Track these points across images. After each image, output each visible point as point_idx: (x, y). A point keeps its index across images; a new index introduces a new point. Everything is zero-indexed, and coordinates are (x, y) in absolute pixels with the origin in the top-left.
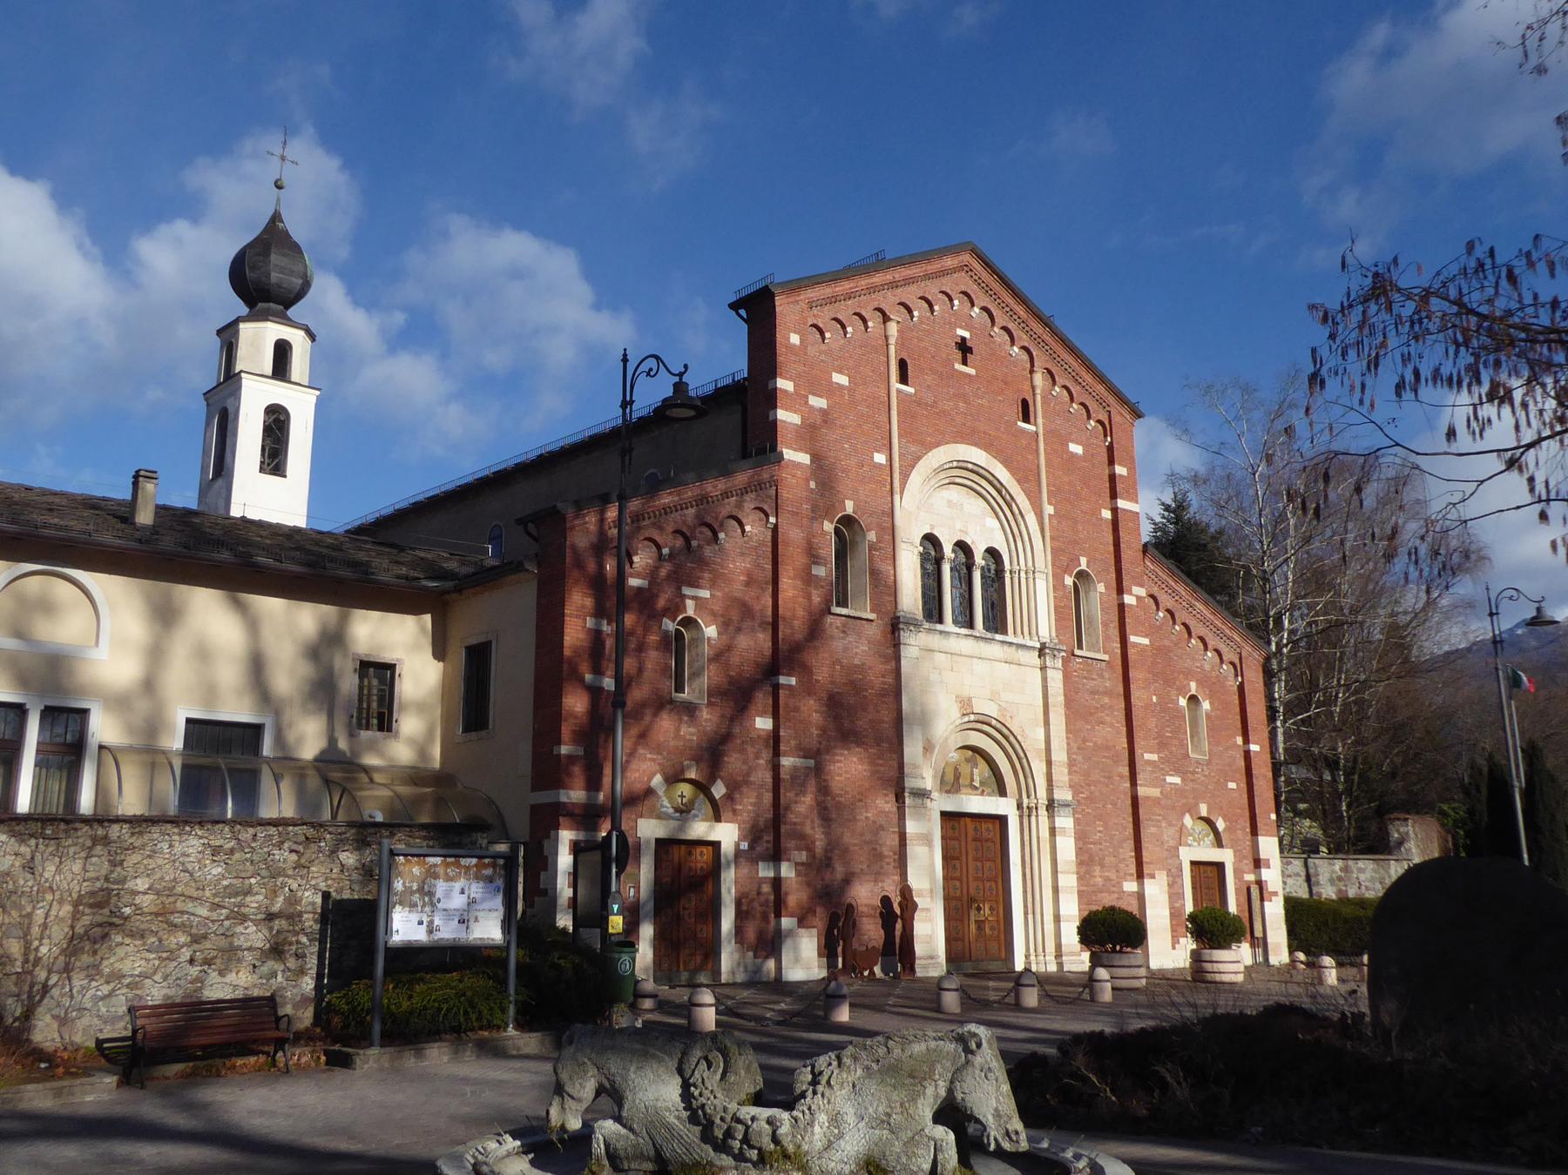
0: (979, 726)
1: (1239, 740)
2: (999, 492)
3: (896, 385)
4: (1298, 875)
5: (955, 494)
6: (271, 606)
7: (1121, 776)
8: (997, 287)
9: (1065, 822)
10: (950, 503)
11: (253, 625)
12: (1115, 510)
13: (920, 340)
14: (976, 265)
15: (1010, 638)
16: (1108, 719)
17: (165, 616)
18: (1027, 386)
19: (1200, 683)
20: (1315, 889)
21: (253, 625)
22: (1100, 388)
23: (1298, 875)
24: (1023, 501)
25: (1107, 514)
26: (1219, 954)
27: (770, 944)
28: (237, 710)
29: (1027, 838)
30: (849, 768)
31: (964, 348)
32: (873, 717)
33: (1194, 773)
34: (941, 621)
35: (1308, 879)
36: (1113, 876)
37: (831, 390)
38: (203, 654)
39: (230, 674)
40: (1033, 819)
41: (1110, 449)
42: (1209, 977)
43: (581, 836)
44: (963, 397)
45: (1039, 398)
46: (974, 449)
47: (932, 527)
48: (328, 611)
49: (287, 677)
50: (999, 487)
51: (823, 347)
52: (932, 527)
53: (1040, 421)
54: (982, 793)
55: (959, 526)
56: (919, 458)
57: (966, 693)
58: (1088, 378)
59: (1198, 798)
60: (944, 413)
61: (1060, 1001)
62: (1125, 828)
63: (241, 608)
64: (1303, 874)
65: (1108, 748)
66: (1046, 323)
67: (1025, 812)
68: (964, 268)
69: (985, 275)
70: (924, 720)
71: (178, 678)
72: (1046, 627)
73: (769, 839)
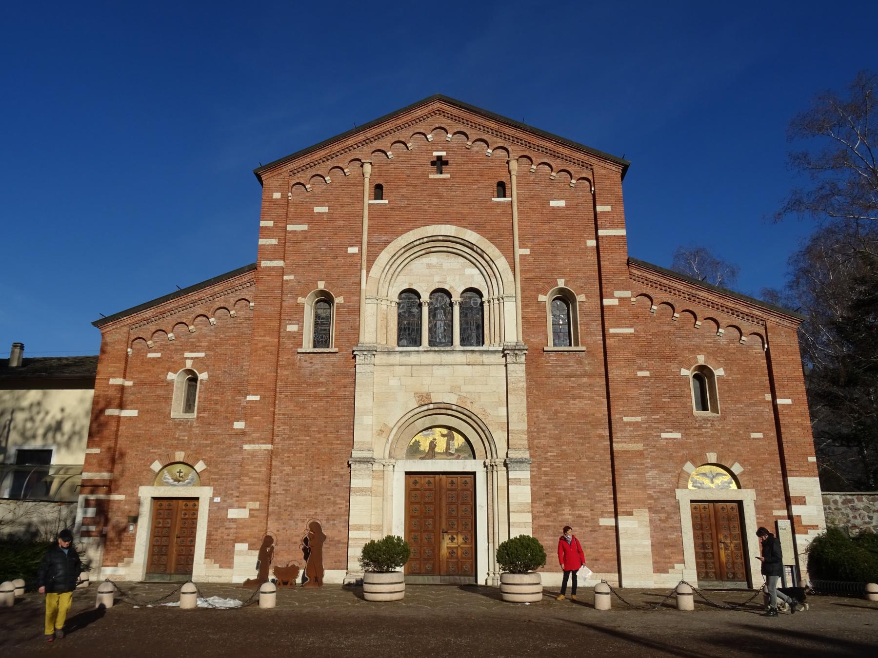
0: (438, 411)
1: (768, 397)
2: (473, 250)
3: (368, 201)
5: (433, 259)
7: (601, 436)
9: (523, 474)
10: (429, 266)
12: (597, 238)
15: (485, 348)
18: (504, 172)
19: (708, 355)
24: (492, 250)
25: (592, 243)
26: (517, 578)
29: (490, 487)
31: (440, 164)
34: (417, 342)
36: (587, 513)
40: (495, 473)
42: (369, 596)
45: (514, 178)
46: (443, 226)
47: (412, 284)
50: (471, 246)
51: (308, 194)
52: (451, 287)
54: (458, 458)
57: (425, 390)
60: (417, 209)
61: (710, 605)
62: (604, 477)
65: (585, 416)
67: (490, 468)
68: (440, 112)
72: (512, 333)
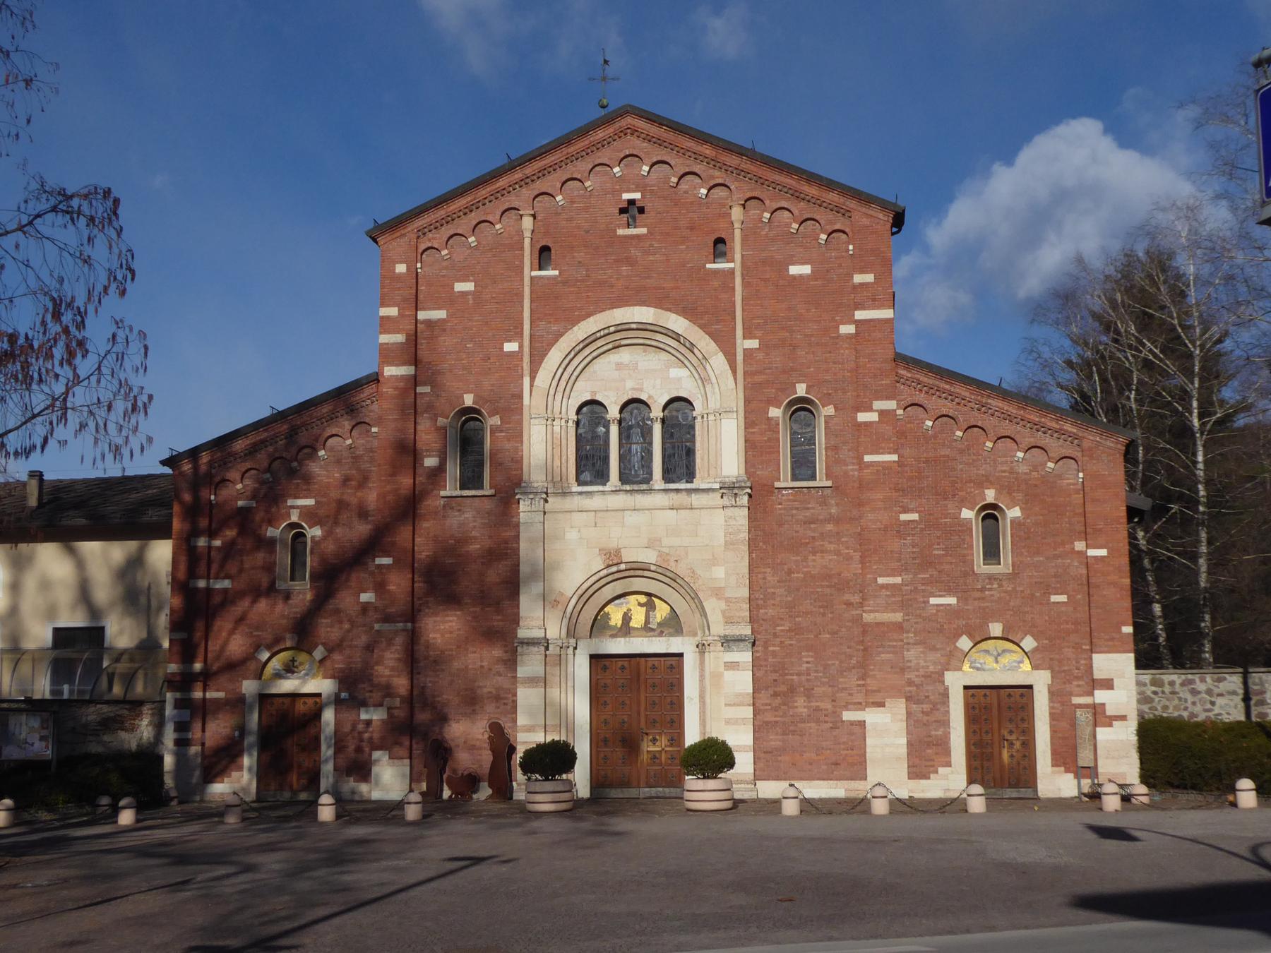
3: (529, 273)
4: (1234, 693)
6: (91, 548)
8: (670, 136)
10: (619, 366)
11: (80, 564)
13: (570, 220)
14: (641, 124)
16: (832, 547)
17: (19, 565)
20: (1255, 711)
21: (80, 564)
22: (833, 197)
23: (1234, 693)
27: (362, 770)
28: (74, 619)
30: (443, 627)
31: (631, 210)
32: (486, 582)
33: (983, 590)
35: (1247, 699)
37: (451, 301)
38: (46, 585)
39: (65, 595)
41: (146, 348)
43: (178, 695)
44: (630, 261)
47: (594, 393)
48: (132, 545)
49: (103, 592)
53: (738, 257)
55: (630, 384)
56: (562, 335)
57: (613, 544)
58: (812, 191)
59: (988, 616)
63: (72, 552)
64: (1241, 691)
66: (740, 151)
67: (702, 648)
69: (654, 130)
70: (541, 574)
71: (31, 600)
73: (353, 688)
